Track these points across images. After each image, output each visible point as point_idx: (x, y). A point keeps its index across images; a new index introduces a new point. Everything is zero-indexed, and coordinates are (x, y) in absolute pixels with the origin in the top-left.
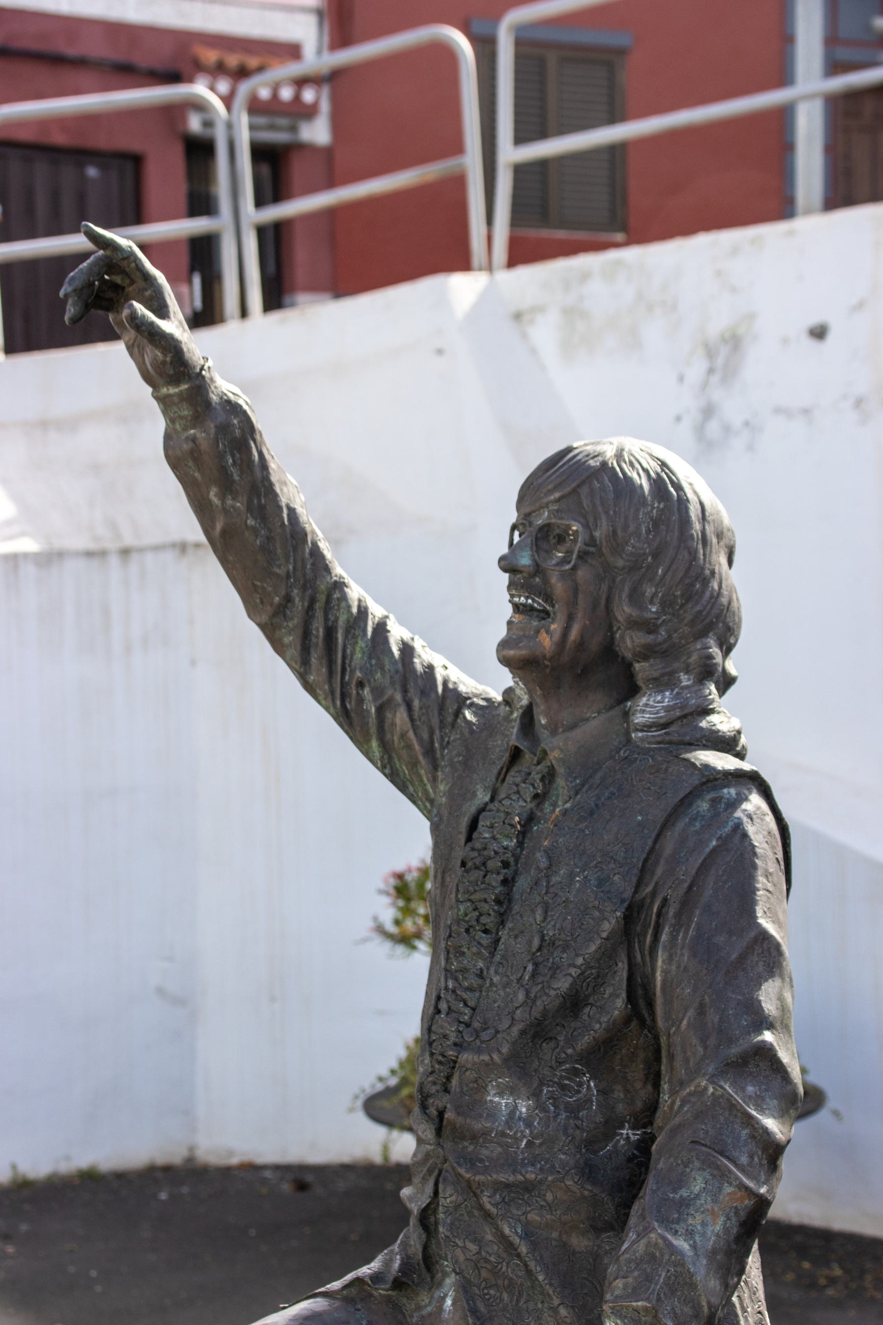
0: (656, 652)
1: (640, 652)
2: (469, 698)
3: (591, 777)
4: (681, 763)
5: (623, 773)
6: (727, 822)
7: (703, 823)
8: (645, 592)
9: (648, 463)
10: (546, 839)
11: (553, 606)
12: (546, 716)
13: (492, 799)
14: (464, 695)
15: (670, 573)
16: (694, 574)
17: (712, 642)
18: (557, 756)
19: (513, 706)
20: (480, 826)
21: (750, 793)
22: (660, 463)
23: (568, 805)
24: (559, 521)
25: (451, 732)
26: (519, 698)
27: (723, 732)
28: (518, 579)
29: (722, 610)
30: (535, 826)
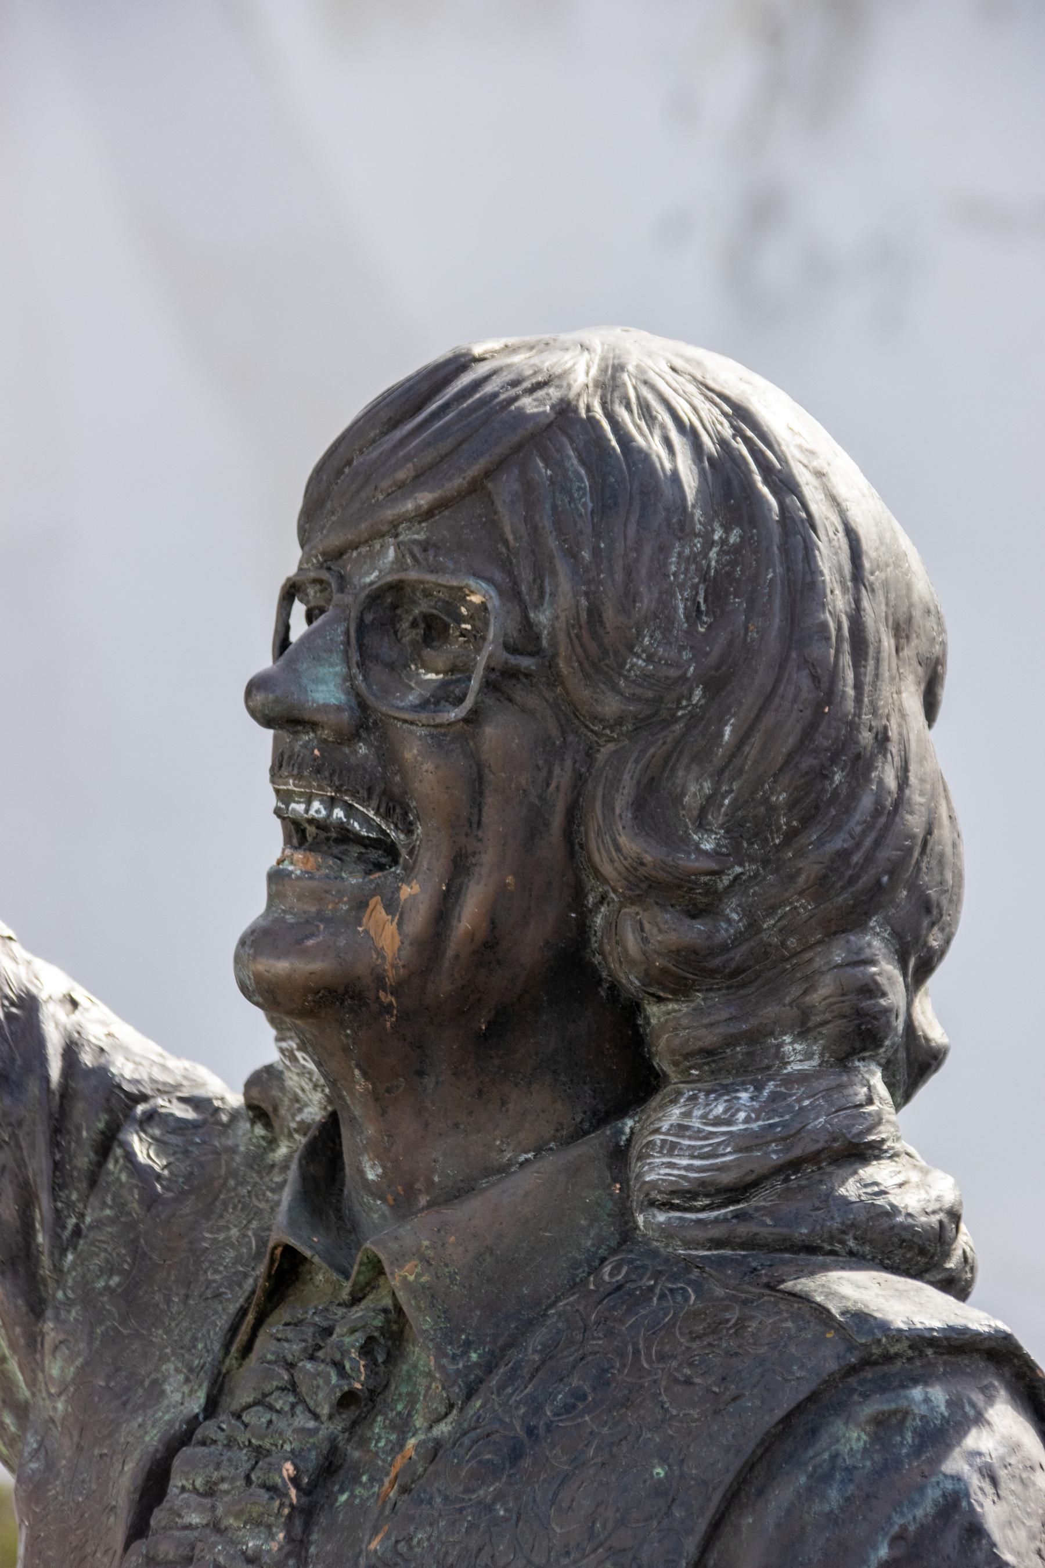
0: (712, 973)
1: (664, 971)
2: (144, 1098)
3: (512, 1343)
4: (782, 1306)
5: (610, 1334)
6: (921, 1489)
7: (851, 1488)
8: (683, 794)
9: (695, 409)
10: (375, 1531)
11: (409, 832)
12: (381, 1155)
13: (211, 1407)
14: (126, 1087)
15: (757, 739)
16: (826, 743)
17: (876, 943)
18: (411, 1278)
19: (276, 1124)
20: (173, 1490)
21: (990, 1400)
22: (729, 410)
23: (443, 1429)
24: (431, 578)
25: (85, 1199)
26: (296, 1099)
27: (909, 1215)
28: (305, 746)
29: (910, 850)
30: (342, 1491)
